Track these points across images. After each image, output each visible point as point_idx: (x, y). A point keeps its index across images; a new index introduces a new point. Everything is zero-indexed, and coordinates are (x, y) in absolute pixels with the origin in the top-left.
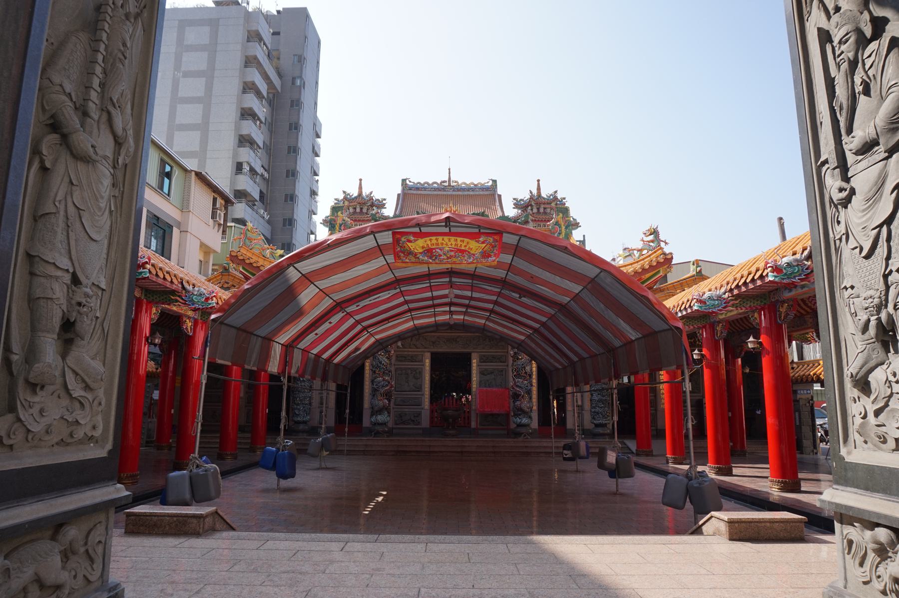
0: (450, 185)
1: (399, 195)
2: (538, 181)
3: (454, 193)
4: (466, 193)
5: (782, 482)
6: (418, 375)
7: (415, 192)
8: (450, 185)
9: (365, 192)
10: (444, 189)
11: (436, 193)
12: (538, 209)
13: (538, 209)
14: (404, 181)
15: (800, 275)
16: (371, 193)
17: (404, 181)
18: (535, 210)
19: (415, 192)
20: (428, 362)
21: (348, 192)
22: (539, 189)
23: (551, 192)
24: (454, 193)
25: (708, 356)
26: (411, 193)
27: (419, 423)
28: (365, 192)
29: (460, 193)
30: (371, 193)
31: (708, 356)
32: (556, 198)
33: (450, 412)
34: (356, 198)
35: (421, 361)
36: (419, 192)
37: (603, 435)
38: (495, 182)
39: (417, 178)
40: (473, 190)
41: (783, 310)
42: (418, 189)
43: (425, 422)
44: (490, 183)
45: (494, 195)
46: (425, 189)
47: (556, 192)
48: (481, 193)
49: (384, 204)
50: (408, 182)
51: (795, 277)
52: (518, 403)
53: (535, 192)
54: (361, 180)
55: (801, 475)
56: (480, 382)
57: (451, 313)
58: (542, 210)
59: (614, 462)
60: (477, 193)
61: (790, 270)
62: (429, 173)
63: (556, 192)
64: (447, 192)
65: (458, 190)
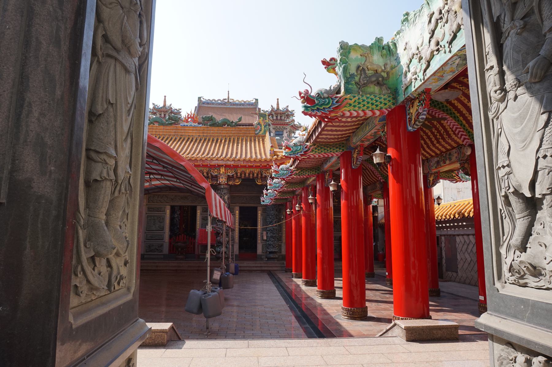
0: (228, 101)
1: (196, 107)
2: (278, 99)
3: (231, 107)
4: (239, 107)
5: (322, 292)
6: (162, 220)
7: (206, 106)
8: (228, 101)
9: (168, 104)
10: (225, 104)
11: (219, 106)
12: (277, 117)
13: (277, 117)
14: (199, 98)
15: (301, 152)
16: (171, 105)
17: (199, 98)
18: (275, 118)
19: (206, 106)
20: (168, 212)
21: (156, 104)
22: (278, 104)
23: (285, 106)
24: (231, 107)
25: (304, 208)
26: (203, 105)
27: (161, 251)
28: (168, 104)
29: (235, 107)
30: (171, 105)
31: (304, 208)
32: (287, 110)
33: (179, 244)
34: (161, 108)
35: (164, 211)
36: (209, 106)
37: (273, 259)
38: (257, 100)
39: (208, 96)
40: (243, 105)
41: (355, 156)
42: (208, 103)
43: (166, 249)
44: (254, 101)
45: (256, 108)
46: (213, 104)
47: (288, 106)
48: (248, 107)
49: (180, 112)
50: (202, 99)
51: (298, 153)
52: (218, 238)
53: (275, 106)
54: (165, 96)
55: (367, 286)
56: (202, 224)
57: (151, 180)
58: (279, 118)
59: (218, 278)
60: (246, 107)
61: (295, 148)
62: (216, 94)
63: (288, 106)
64: (227, 106)
65: (234, 105)
